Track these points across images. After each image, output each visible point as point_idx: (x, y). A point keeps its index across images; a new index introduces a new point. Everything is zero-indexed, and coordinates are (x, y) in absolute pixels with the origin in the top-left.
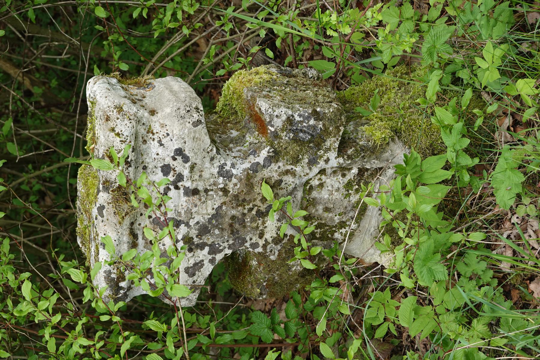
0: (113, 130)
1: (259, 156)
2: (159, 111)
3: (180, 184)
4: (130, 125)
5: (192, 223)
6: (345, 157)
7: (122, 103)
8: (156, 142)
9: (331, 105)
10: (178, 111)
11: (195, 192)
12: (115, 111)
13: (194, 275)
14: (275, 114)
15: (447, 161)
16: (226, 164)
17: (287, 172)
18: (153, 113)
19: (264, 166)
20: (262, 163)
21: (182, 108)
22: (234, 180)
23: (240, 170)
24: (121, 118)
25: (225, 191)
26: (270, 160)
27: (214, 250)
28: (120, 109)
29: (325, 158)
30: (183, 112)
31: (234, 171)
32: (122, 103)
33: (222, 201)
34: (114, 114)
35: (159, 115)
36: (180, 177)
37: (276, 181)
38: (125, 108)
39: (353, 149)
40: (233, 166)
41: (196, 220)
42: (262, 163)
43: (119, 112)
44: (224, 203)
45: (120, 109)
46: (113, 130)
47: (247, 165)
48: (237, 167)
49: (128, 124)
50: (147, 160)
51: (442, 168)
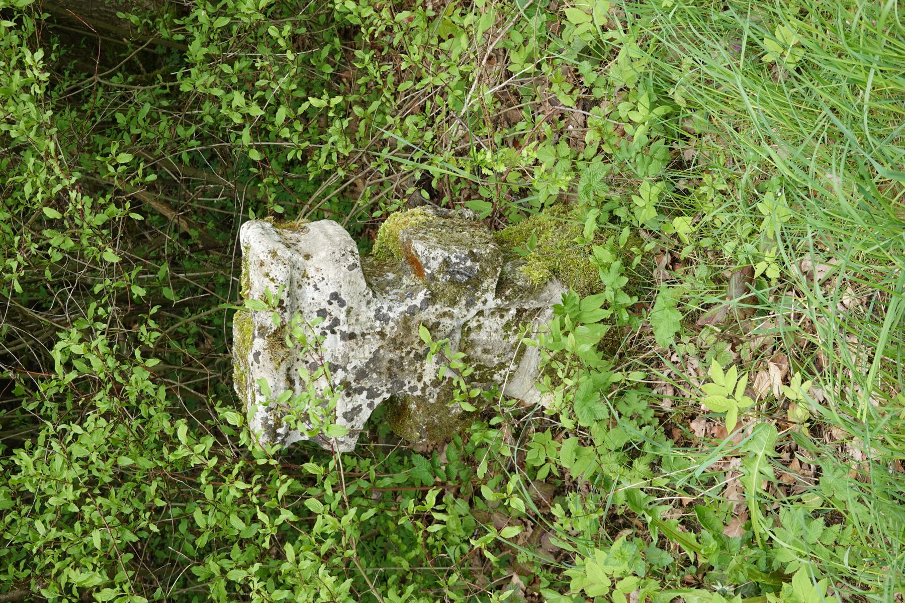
0: (267, 275)
3: (336, 329)
5: (349, 367)
11: (352, 336)
13: (352, 419)
16: (382, 308)
18: (307, 257)
21: (337, 251)
22: (391, 324)
23: (397, 313)
24: (275, 263)
25: (382, 334)
26: (427, 302)
27: (372, 394)
28: (274, 254)
29: (483, 299)
30: (338, 256)
31: (391, 315)
33: (380, 344)
34: (268, 259)
35: (314, 259)
38: (279, 253)
40: (390, 309)
43: (273, 257)
44: (382, 347)
45: (274, 254)
46: (267, 275)
47: (404, 308)
49: (283, 269)
50: (303, 305)
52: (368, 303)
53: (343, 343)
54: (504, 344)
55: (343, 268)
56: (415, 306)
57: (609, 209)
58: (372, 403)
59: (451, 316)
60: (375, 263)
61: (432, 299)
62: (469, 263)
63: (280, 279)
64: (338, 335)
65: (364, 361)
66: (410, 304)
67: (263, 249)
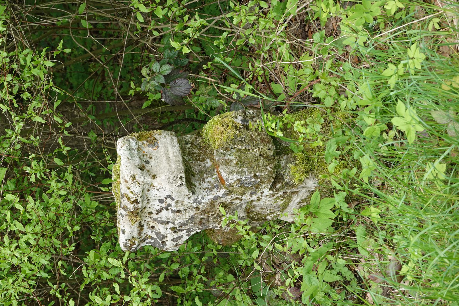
0: (129, 189)
1: (219, 191)
2: (158, 176)
3: (169, 208)
4: (139, 188)
5: (176, 223)
6: (275, 190)
7: (135, 174)
8: (155, 190)
9: (266, 169)
10: (169, 180)
11: (179, 211)
12: (131, 179)
13: (177, 241)
14: (230, 178)
15: (335, 205)
16: (198, 198)
17: (237, 198)
18: (154, 177)
19: (222, 197)
20: (221, 196)
21: (172, 178)
22: (203, 204)
23: (207, 200)
24: (134, 183)
25: (197, 208)
26: (226, 194)
27: (189, 231)
28: (133, 178)
29: (261, 191)
30: (172, 181)
31: (203, 201)
32: (135, 174)
33: (195, 213)
34: (130, 181)
35: (158, 179)
36: (170, 205)
37: (229, 203)
38: (137, 177)
39: (281, 184)
40: (203, 198)
41: (178, 222)
42: (221, 196)
43: (133, 180)
44: (197, 213)
45: (133, 178)
46: (129, 189)
47: (212, 197)
48: (205, 198)
49: (138, 188)
50: (150, 197)
51: (331, 210)
52: (189, 198)
53: (173, 214)
54: (274, 205)
55: (174, 186)
56: (218, 196)
57: (348, 209)
58: (190, 234)
59: (241, 200)
60: (202, 145)
61: (229, 193)
62: (253, 180)
63: (136, 192)
64: (170, 211)
65: (185, 220)
66: (215, 195)
67: (128, 173)
